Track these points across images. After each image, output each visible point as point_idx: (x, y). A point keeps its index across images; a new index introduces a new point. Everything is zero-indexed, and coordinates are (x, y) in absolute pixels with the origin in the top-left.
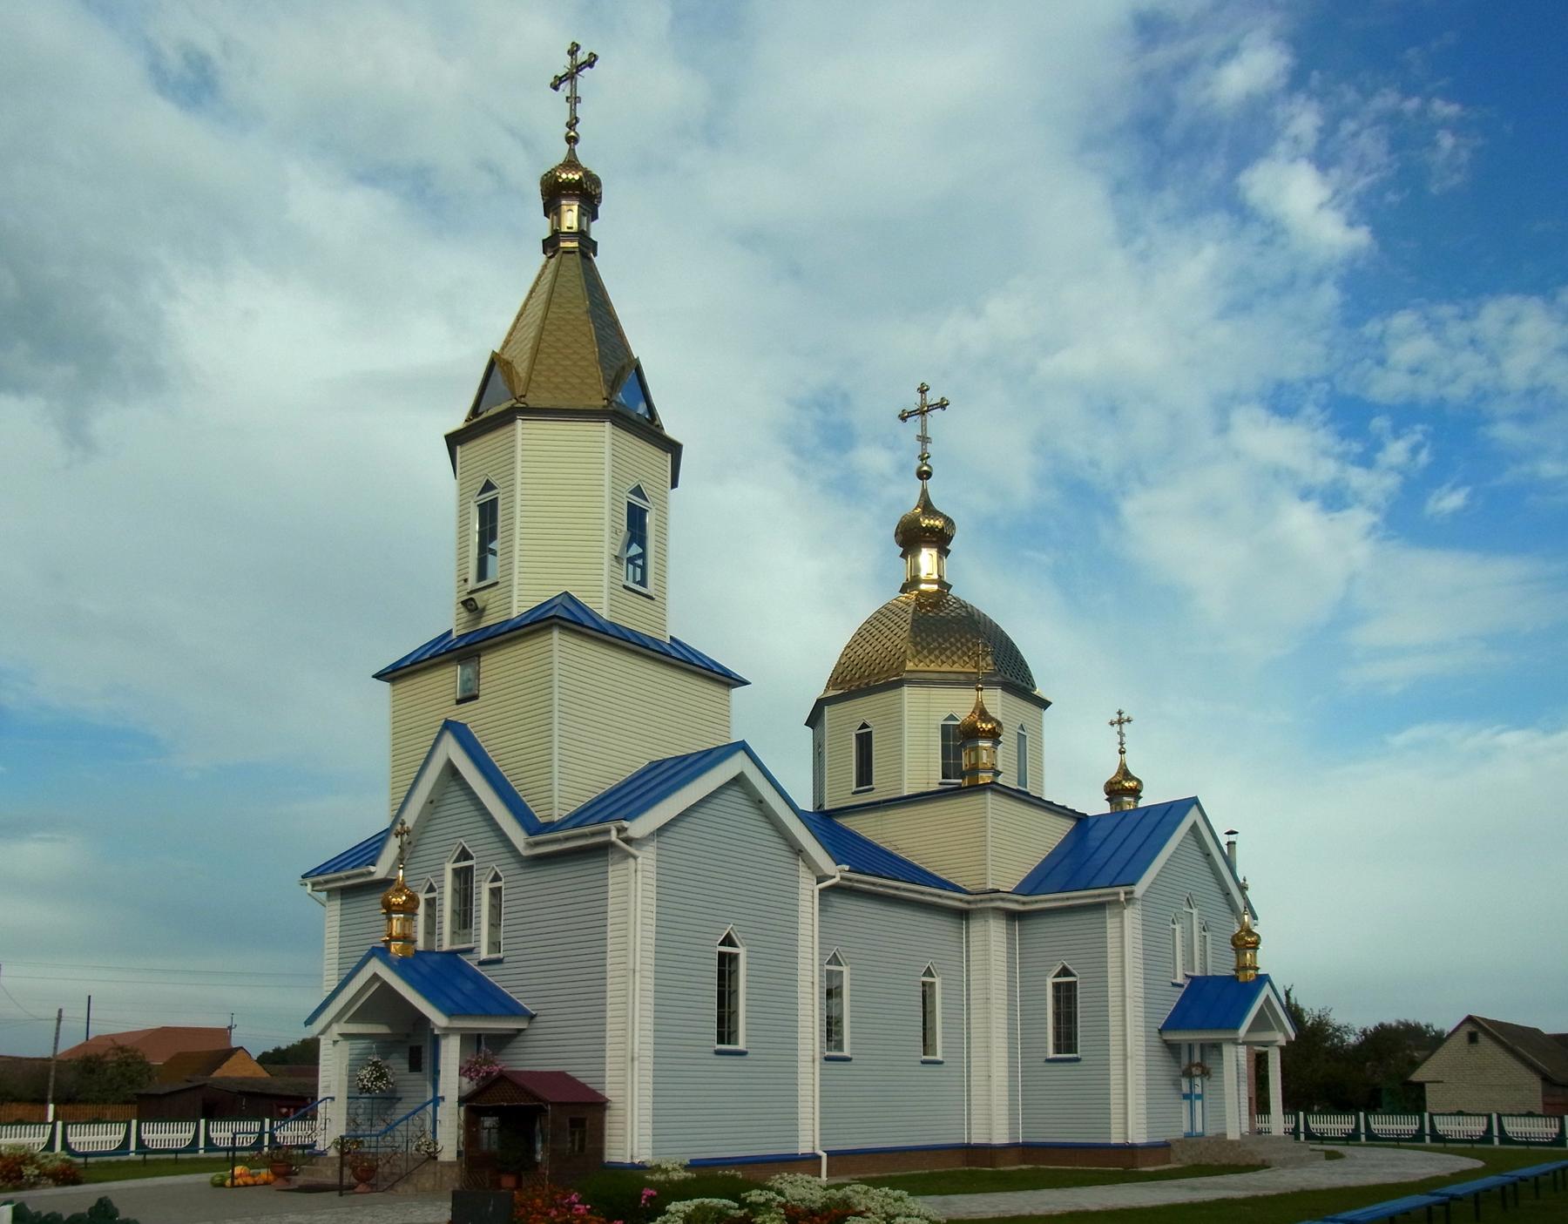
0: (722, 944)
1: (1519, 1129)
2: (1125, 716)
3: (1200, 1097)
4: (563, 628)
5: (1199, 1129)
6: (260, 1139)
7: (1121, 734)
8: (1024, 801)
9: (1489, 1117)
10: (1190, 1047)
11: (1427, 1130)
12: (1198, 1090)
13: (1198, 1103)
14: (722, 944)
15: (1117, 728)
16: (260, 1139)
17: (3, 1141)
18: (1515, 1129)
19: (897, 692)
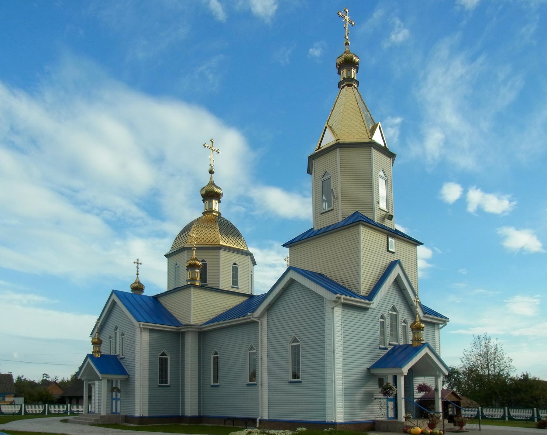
0: (161, 355)
1: (31, 409)
2: (136, 261)
3: (119, 399)
4: (363, 225)
5: (119, 411)
6: (478, 412)
7: (137, 267)
8: (185, 289)
9: (21, 405)
10: (117, 381)
11: (69, 410)
12: (119, 397)
13: (119, 402)
14: (161, 355)
15: (136, 265)
16: (478, 412)
17: (546, 415)
18: (29, 409)
19: (352, 231)
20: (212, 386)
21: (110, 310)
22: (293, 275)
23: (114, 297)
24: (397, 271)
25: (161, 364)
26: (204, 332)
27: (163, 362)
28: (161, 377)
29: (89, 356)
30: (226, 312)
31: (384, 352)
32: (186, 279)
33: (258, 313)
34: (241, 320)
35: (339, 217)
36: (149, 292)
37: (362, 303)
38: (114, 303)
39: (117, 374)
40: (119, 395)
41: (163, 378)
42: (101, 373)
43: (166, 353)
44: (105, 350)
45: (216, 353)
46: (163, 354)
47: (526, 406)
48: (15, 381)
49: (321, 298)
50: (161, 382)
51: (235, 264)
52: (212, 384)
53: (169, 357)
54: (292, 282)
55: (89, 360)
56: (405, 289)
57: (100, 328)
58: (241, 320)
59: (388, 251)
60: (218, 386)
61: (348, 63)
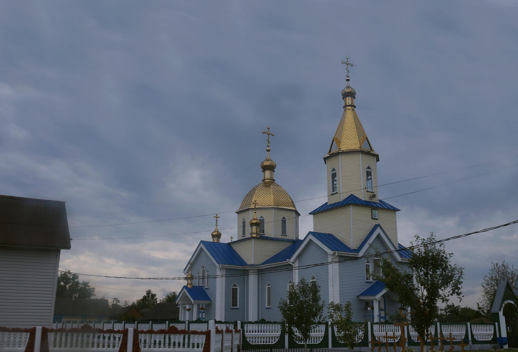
15: (215, 218)
20: (267, 308)
21: (198, 255)
22: (311, 237)
23: (202, 245)
24: (378, 231)
25: (233, 293)
26: (262, 270)
27: (235, 291)
28: (233, 302)
29: (185, 287)
30: (277, 255)
31: (371, 285)
32: (250, 232)
33: (292, 260)
34: (283, 263)
35: (342, 197)
36: (225, 239)
37: (353, 254)
38: (202, 249)
39: (204, 300)
40: (204, 314)
41: (234, 303)
42: (194, 300)
43: (237, 285)
44: (196, 283)
45: (269, 285)
46: (235, 285)
47: (163, 321)
48: (91, 298)
49: (326, 253)
50: (233, 306)
51: (284, 218)
52: (267, 307)
53: (238, 288)
54: (311, 241)
55: (185, 290)
56: (385, 242)
57: (192, 265)
58: (283, 263)
59: (372, 218)
60: (270, 308)
61: (350, 94)
